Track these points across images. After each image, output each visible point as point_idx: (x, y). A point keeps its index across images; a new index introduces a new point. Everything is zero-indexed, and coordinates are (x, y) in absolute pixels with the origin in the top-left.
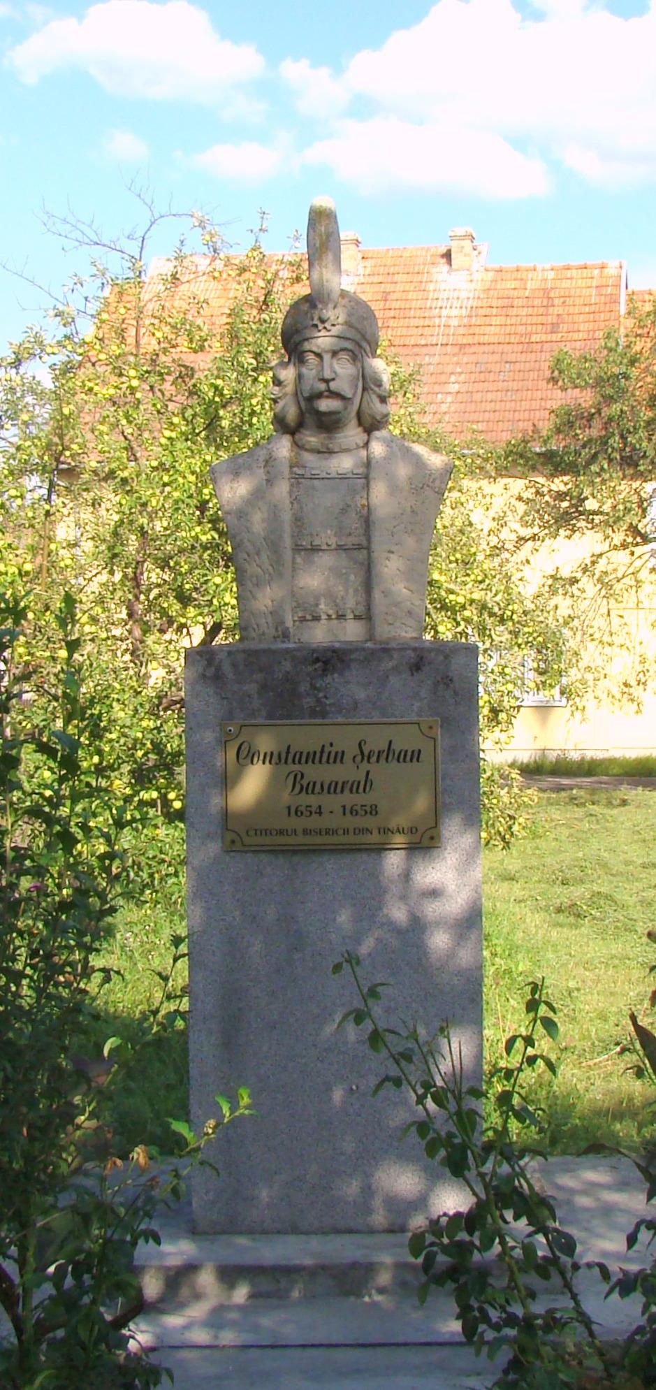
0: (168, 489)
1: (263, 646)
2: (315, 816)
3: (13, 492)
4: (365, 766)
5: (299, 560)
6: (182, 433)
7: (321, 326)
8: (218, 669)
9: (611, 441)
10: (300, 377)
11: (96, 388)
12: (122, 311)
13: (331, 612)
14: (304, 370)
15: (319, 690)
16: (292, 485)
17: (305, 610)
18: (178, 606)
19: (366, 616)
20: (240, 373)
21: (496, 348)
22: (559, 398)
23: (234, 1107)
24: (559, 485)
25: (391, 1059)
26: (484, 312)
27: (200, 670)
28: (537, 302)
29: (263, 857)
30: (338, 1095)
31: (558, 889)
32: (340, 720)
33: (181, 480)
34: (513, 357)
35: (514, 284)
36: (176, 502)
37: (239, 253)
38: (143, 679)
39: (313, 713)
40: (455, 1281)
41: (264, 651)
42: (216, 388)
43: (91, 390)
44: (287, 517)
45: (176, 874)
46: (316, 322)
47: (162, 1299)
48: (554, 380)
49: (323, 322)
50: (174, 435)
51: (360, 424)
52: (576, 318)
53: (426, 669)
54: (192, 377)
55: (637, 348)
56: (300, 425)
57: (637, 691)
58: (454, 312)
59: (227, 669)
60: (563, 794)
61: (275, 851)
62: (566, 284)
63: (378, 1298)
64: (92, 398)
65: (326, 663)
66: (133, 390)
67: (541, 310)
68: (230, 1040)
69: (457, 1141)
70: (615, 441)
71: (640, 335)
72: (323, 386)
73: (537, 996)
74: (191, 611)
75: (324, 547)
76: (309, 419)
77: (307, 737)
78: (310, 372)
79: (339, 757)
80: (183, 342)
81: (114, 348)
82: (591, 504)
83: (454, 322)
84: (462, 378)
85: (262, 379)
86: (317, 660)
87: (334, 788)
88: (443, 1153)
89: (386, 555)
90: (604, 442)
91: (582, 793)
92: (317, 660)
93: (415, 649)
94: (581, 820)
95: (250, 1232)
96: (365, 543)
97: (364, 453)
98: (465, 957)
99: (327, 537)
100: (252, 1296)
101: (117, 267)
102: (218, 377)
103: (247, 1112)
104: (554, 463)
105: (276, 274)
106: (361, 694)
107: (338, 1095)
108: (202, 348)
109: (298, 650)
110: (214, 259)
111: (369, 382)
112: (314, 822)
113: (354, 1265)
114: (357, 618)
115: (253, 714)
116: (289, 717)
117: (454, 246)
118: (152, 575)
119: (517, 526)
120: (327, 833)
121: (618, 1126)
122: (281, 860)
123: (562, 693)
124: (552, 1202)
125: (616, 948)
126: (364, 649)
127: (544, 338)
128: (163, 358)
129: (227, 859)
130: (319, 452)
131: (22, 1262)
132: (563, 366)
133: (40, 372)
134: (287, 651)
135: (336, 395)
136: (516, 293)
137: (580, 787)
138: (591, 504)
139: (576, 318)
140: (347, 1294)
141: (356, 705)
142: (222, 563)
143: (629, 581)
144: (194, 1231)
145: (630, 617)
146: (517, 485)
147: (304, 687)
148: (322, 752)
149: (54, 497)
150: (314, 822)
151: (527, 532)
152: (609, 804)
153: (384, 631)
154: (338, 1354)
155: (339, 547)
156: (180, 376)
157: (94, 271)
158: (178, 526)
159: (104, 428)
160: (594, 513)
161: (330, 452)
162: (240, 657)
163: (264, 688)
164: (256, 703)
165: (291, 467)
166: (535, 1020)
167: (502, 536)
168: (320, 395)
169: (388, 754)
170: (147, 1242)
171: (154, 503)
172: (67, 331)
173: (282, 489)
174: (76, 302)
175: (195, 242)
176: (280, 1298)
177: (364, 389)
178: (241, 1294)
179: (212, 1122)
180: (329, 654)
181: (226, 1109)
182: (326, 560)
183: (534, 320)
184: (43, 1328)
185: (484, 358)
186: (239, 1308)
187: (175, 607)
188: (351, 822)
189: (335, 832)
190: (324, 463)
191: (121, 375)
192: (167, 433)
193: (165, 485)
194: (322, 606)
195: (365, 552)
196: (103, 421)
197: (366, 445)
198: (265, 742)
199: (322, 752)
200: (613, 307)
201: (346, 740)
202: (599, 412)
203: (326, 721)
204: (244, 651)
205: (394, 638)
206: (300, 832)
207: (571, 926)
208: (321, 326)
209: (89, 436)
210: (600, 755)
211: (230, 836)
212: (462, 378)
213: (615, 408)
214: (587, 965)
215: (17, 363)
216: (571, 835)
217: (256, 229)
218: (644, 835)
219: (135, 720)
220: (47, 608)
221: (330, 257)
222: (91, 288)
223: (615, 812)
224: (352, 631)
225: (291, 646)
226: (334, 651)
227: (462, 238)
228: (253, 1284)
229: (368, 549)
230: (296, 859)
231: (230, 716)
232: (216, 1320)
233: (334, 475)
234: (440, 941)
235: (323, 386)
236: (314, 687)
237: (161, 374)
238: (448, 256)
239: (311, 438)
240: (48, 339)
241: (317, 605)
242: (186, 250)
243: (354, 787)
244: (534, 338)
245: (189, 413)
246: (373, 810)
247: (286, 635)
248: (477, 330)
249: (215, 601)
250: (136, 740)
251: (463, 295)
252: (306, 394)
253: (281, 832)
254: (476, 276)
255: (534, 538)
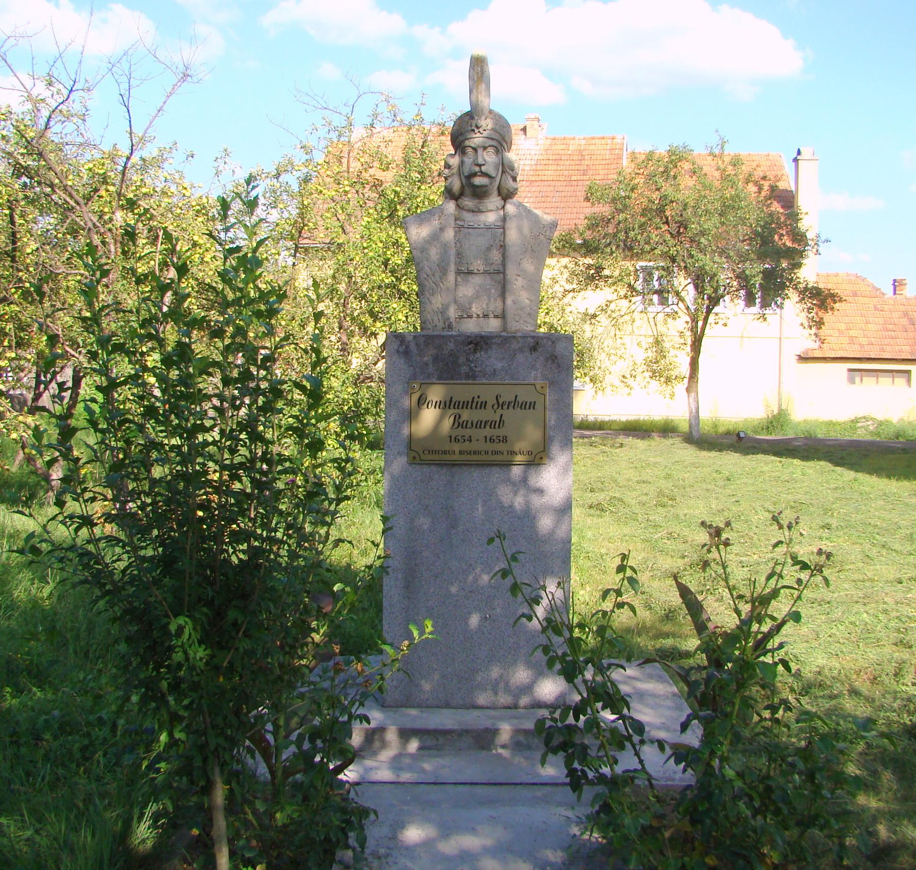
0: (366, 251)
1: (436, 333)
2: (467, 443)
3: (273, 251)
4: (499, 411)
5: (459, 279)
6: (375, 219)
7: (476, 131)
8: (407, 347)
9: (619, 235)
10: (462, 162)
11: (324, 191)
12: (341, 146)
13: (479, 313)
14: (466, 159)
15: (472, 362)
16: (456, 232)
17: (463, 311)
18: (370, 321)
19: (503, 316)
20: (410, 184)
21: (551, 183)
22: (589, 210)
23: (422, 632)
24: (588, 261)
25: (526, 603)
26: (544, 162)
27: (396, 347)
28: (575, 158)
29: (433, 467)
30: (474, 620)
31: (589, 495)
32: (485, 381)
33: (374, 246)
34: (561, 189)
35: (562, 147)
36: (371, 259)
37: (408, 118)
38: (348, 363)
39: (468, 377)
40: (566, 751)
41: (437, 336)
42: (396, 192)
43: (321, 192)
44: (452, 252)
45: (366, 480)
46: (474, 128)
47: (362, 749)
48: (587, 199)
49: (478, 128)
50: (370, 220)
51: (499, 194)
52: (598, 167)
53: (540, 350)
54: (381, 186)
55: (636, 181)
56: (462, 194)
57: (630, 381)
58: (527, 162)
59: (413, 347)
60: (586, 440)
61: (441, 464)
62: (592, 147)
63: (500, 751)
64: (321, 197)
65: (476, 345)
66: (346, 193)
67: (578, 162)
68: (409, 585)
69: (568, 658)
70: (622, 236)
71: (639, 174)
72: (477, 169)
73: (625, 563)
74: (378, 324)
75: (476, 271)
76: (468, 191)
77: (464, 392)
78: (468, 160)
79: (484, 405)
80: (376, 164)
81: (335, 168)
82: (606, 272)
83: (528, 168)
84: (531, 200)
85: (423, 187)
86: (471, 343)
87: (480, 425)
88: (558, 666)
89: (516, 277)
90: (615, 235)
91: (597, 439)
92: (471, 343)
93: (533, 337)
94: (598, 455)
95: (419, 706)
96: (502, 270)
97: (502, 213)
98: (561, 533)
99: (478, 265)
100: (421, 748)
101: (338, 121)
102: (396, 186)
103: (430, 636)
104: (589, 248)
105: (430, 130)
106: (499, 365)
107: (474, 620)
108: (388, 168)
109: (459, 336)
110: (394, 121)
111: (507, 168)
112: (467, 446)
113: (487, 730)
114: (496, 317)
115: (429, 377)
116: (452, 378)
117: (528, 124)
118: (354, 304)
119: (564, 283)
120: (474, 453)
121: (639, 640)
122: (445, 470)
123: (591, 380)
124: (628, 699)
125: (626, 530)
126: (501, 336)
127: (579, 178)
128: (364, 174)
129: (410, 468)
130: (473, 212)
131: (275, 733)
132: (593, 191)
133: (292, 180)
134: (451, 336)
135: (485, 175)
136: (563, 152)
137: (595, 436)
138: (606, 272)
139: (598, 167)
140: (483, 748)
141: (494, 373)
142: (397, 296)
143: (627, 318)
144: (383, 706)
145: (627, 340)
146: (565, 261)
147: (462, 360)
148: (473, 402)
149: (298, 255)
150: (467, 446)
151: (569, 287)
152: (612, 446)
153: (513, 326)
154: (479, 790)
155: (485, 272)
156: (374, 185)
157: (324, 122)
158: (371, 273)
159: (329, 215)
160: (607, 277)
161: (480, 211)
162: (422, 340)
163: (436, 359)
164: (431, 368)
165: (456, 220)
166: (623, 579)
167: (555, 289)
168: (474, 175)
169: (515, 403)
170: (361, 722)
171: (358, 259)
172: (308, 157)
173: (450, 234)
174: (312, 142)
175: (383, 108)
176: (438, 750)
177: (503, 172)
178: (413, 746)
179: (406, 643)
180: (478, 339)
181: (416, 633)
182: (477, 280)
183: (574, 167)
184: (288, 773)
185: (545, 189)
186: (412, 756)
187: (369, 321)
188: (490, 447)
189: (479, 453)
190: (476, 218)
191: (339, 184)
192: (366, 219)
193: (364, 248)
194: (474, 309)
195: (502, 275)
196: (328, 210)
197: (503, 207)
198: (436, 393)
199: (473, 402)
200: (619, 161)
201: (487, 394)
202: (613, 218)
203: (477, 382)
204: (424, 336)
205: (519, 331)
206: (457, 452)
207: (598, 516)
208: (476, 131)
209: (319, 218)
210: (607, 419)
211: (413, 454)
212: (531, 200)
213: (621, 217)
214: (610, 540)
215: (277, 176)
216: (593, 463)
217: (419, 104)
218: (635, 464)
219: (344, 388)
220: (293, 318)
221: (483, 86)
222: (322, 132)
223: (617, 450)
224: (493, 325)
225: (454, 333)
226: (482, 337)
227: (533, 120)
228: (420, 739)
229: (504, 273)
230: (455, 469)
231: (414, 377)
232: (396, 763)
233: (482, 226)
234: (545, 523)
235: (477, 169)
236: (468, 360)
237: (363, 184)
238: (524, 130)
239: (468, 202)
240: (296, 162)
241: (470, 308)
242: (379, 110)
243: (493, 424)
244: (573, 178)
245: (379, 207)
246: (505, 440)
247: (450, 327)
248: (540, 173)
249: (393, 318)
250: (344, 400)
251: (533, 152)
252: (466, 174)
253: (445, 452)
254: (540, 142)
255: (573, 290)
